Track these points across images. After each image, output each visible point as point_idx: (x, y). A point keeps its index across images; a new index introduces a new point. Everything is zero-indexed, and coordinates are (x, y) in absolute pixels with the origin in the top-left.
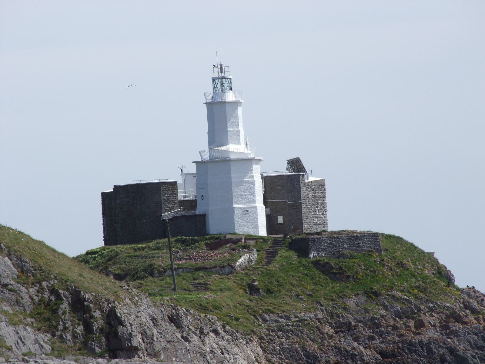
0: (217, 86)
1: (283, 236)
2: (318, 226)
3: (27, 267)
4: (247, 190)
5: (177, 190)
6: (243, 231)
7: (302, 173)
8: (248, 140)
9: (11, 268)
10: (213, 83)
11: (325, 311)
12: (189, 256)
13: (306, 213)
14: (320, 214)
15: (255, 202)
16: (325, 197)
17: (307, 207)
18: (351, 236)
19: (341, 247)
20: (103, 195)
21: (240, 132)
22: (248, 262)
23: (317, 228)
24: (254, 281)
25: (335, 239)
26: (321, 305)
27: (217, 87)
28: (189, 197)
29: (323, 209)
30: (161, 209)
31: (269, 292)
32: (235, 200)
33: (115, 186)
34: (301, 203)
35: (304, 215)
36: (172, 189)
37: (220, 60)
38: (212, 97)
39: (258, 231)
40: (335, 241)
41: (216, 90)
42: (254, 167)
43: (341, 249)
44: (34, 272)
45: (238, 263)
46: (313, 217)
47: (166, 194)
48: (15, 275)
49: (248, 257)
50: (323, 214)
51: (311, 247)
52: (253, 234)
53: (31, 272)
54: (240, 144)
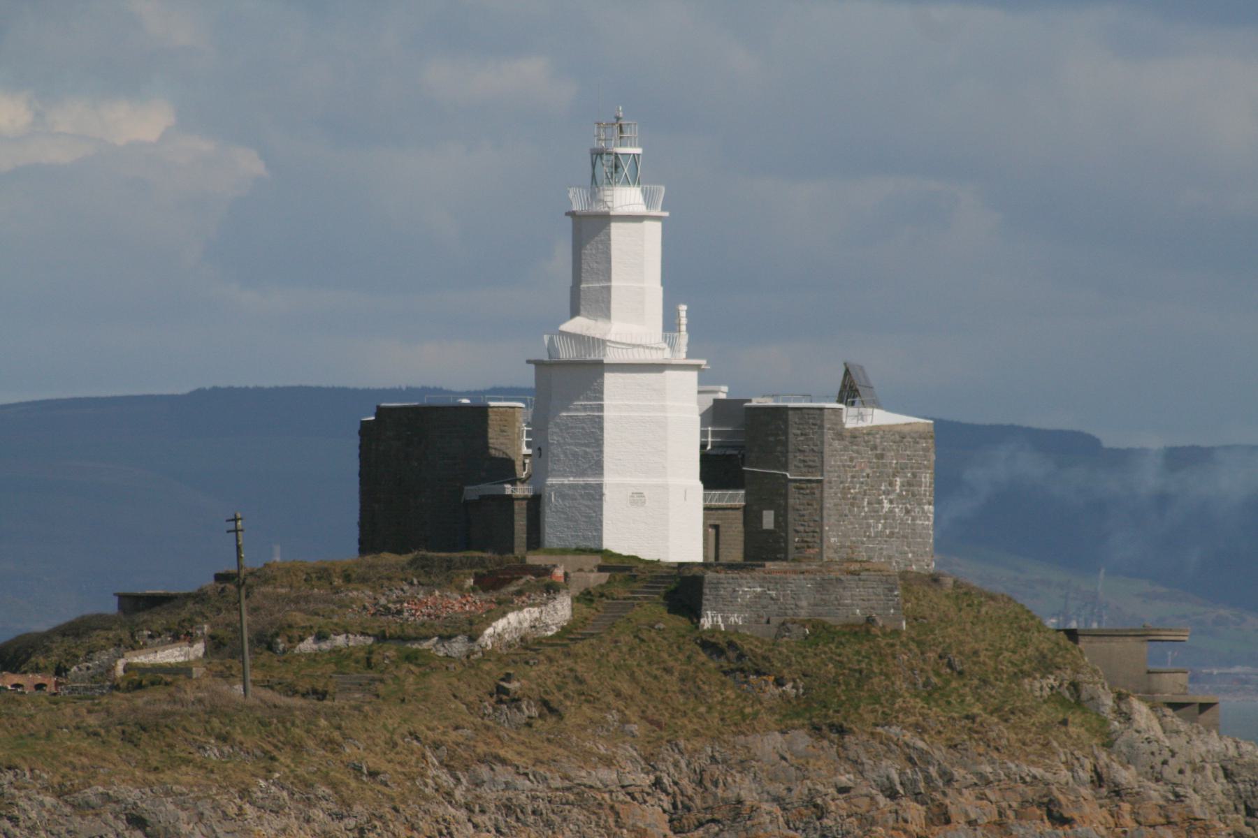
15: (601, 467)
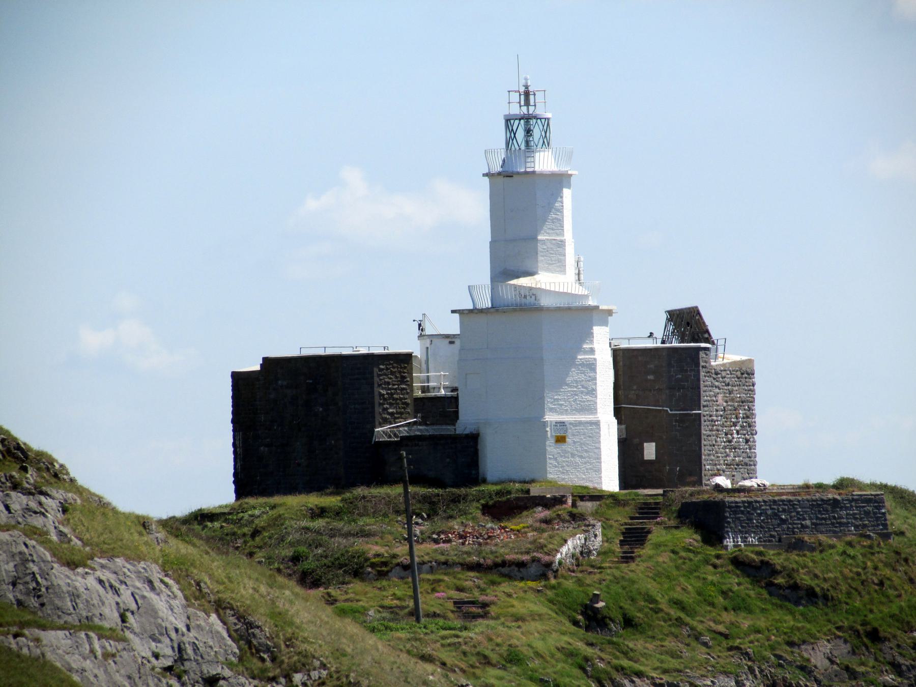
0: (516, 135)
1: (660, 491)
2: (736, 469)
3: (260, 638)
4: (576, 381)
5: (411, 373)
6: (566, 477)
7: (703, 345)
8: (582, 263)
9: (224, 639)
10: (507, 126)
11: (757, 673)
12: (443, 532)
13: (710, 438)
14: (741, 440)
16: (753, 402)
17: (713, 423)
18: (822, 500)
19: (798, 524)
20: (237, 378)
21: (565, 246)
22: (582, 553)
23: (734, 473)
24: (596, 598)
25: (785, 505)
26: (750, 659)
27: (515, 136)
28: (438, 389)
29: (749, 429)
30: (374, 417)
31: (628, 622)
32: (548, 404)
33: (265, 359)
34: (700, 414)
35: (705, 443)
36: (400, 372)
37: (524, 76)
38: (504, 161)
39: (600, 478)
40: (784, 511)
41: (513, 143)
42: (597, 330)
43: (798, 528)
44: (274, 651)
45: (559, 556)
46: (725, 448)
47: (385, 381)
48: (231, 656)
49: (583, 541)
50: (747, 441)
51: (729, 523)
52: (590, 485)
53: (268, 650)
54: (565, 274)
